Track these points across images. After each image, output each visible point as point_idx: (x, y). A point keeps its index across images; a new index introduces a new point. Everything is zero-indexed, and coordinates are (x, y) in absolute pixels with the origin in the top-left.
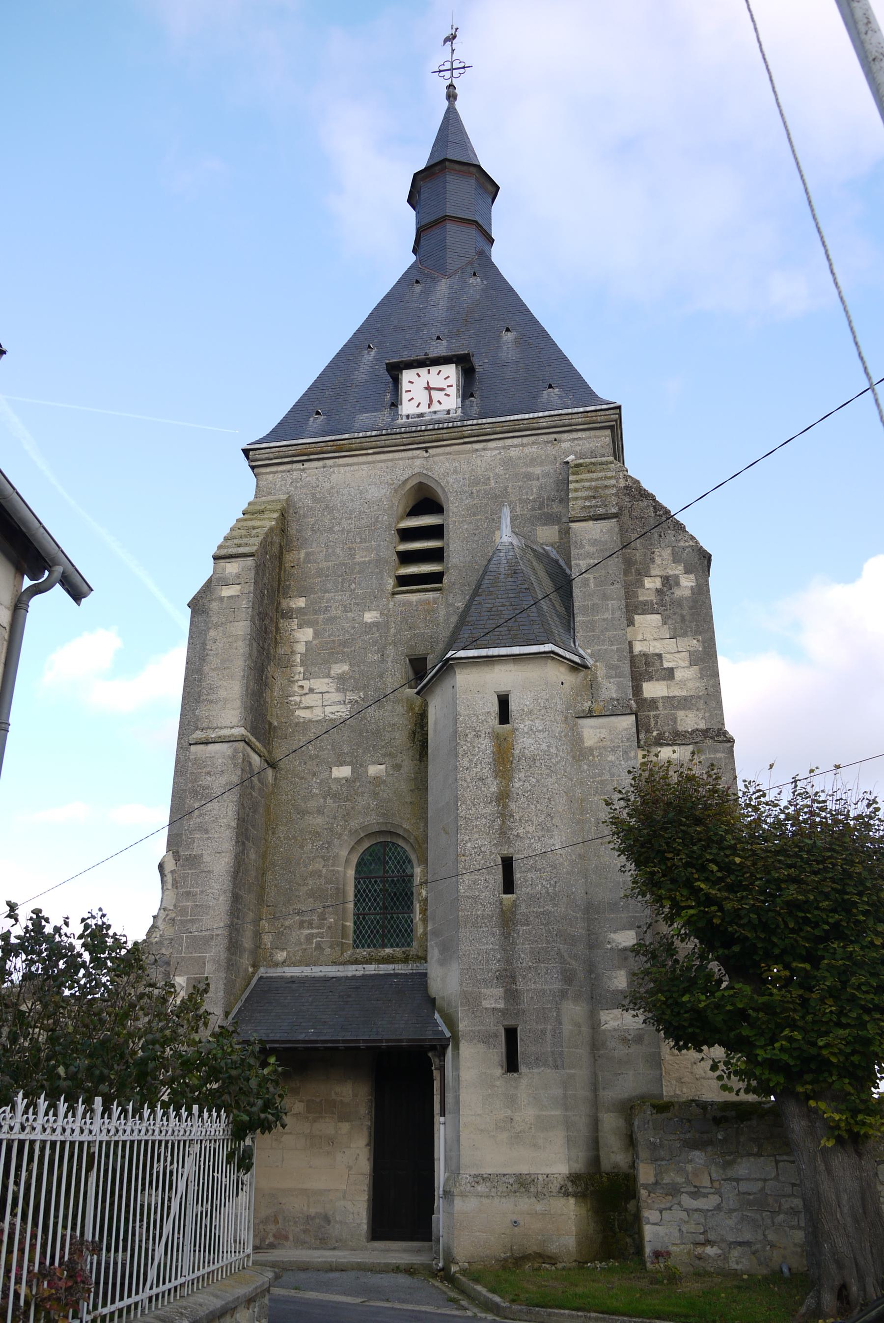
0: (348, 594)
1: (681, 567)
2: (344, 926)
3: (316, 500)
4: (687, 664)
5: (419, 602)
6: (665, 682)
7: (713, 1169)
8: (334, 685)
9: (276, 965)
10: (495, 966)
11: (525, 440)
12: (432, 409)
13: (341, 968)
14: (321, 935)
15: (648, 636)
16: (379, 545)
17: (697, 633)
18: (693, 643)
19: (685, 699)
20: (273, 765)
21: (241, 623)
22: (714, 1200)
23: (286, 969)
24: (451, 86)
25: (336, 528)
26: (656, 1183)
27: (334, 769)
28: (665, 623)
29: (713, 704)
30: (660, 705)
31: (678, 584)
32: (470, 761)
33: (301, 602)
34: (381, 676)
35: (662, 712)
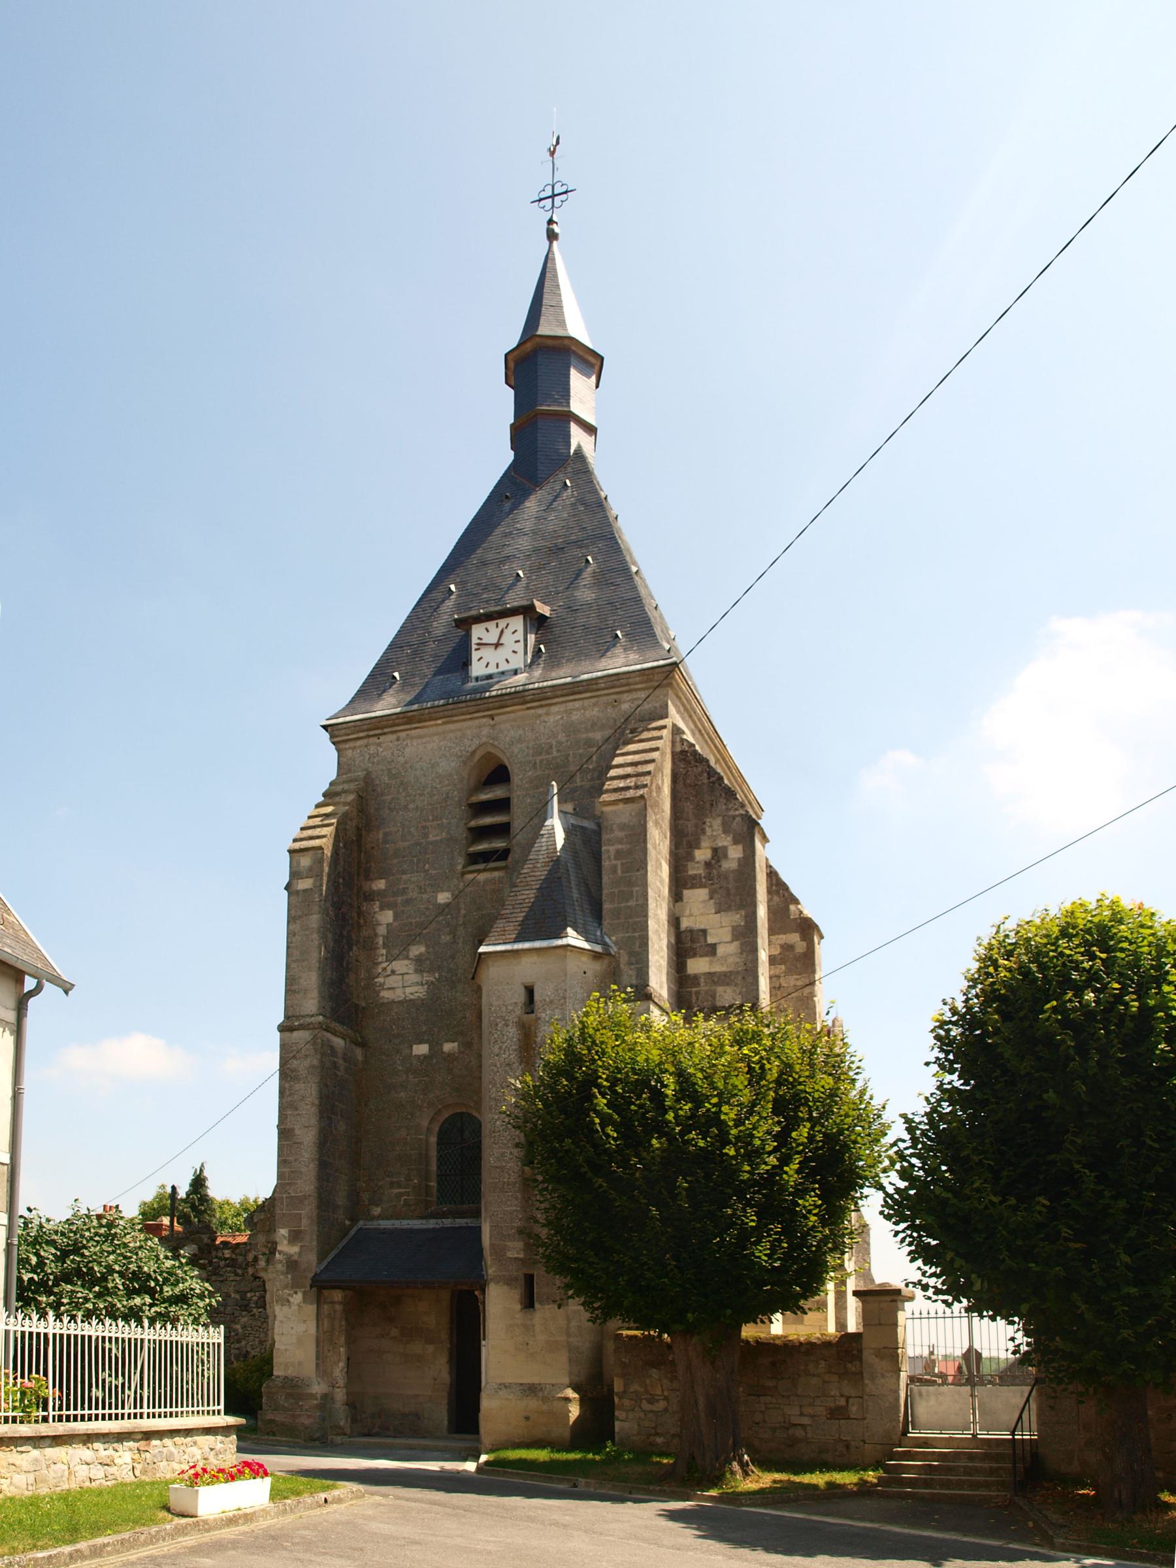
0: (422, 875)
1: (729, 839)
2: (427, 1186)
3: (392, 776)
4: (728, 938)
5: (486, 881)
6: (707, 959)
7: (665, 1381)
8: (412, 967)
9: (373, 1218)
10: (518, 1224)
11: (586, 702)
12: (501, 669)
13: (424, 1221)
14: (408, 1194)
15: (695, 911)
16: (450, 823)
17: (740, 907)
18: (737, 918)
19: (725, 974)
20: (363, 1044)
21: (315, 916)
22: (662, 1405)
23: (381, 1222)
24: (551, 222)
25: (411, 806)
26: (625, 1392)
27: (415, 1047)
28: (711, 898)
29: (750, 979)
30: (702, 980)
31: (726, 856)
32: (500, 1048)
33: (381, 885)
34: (453, 957)
35: (703, 988)
